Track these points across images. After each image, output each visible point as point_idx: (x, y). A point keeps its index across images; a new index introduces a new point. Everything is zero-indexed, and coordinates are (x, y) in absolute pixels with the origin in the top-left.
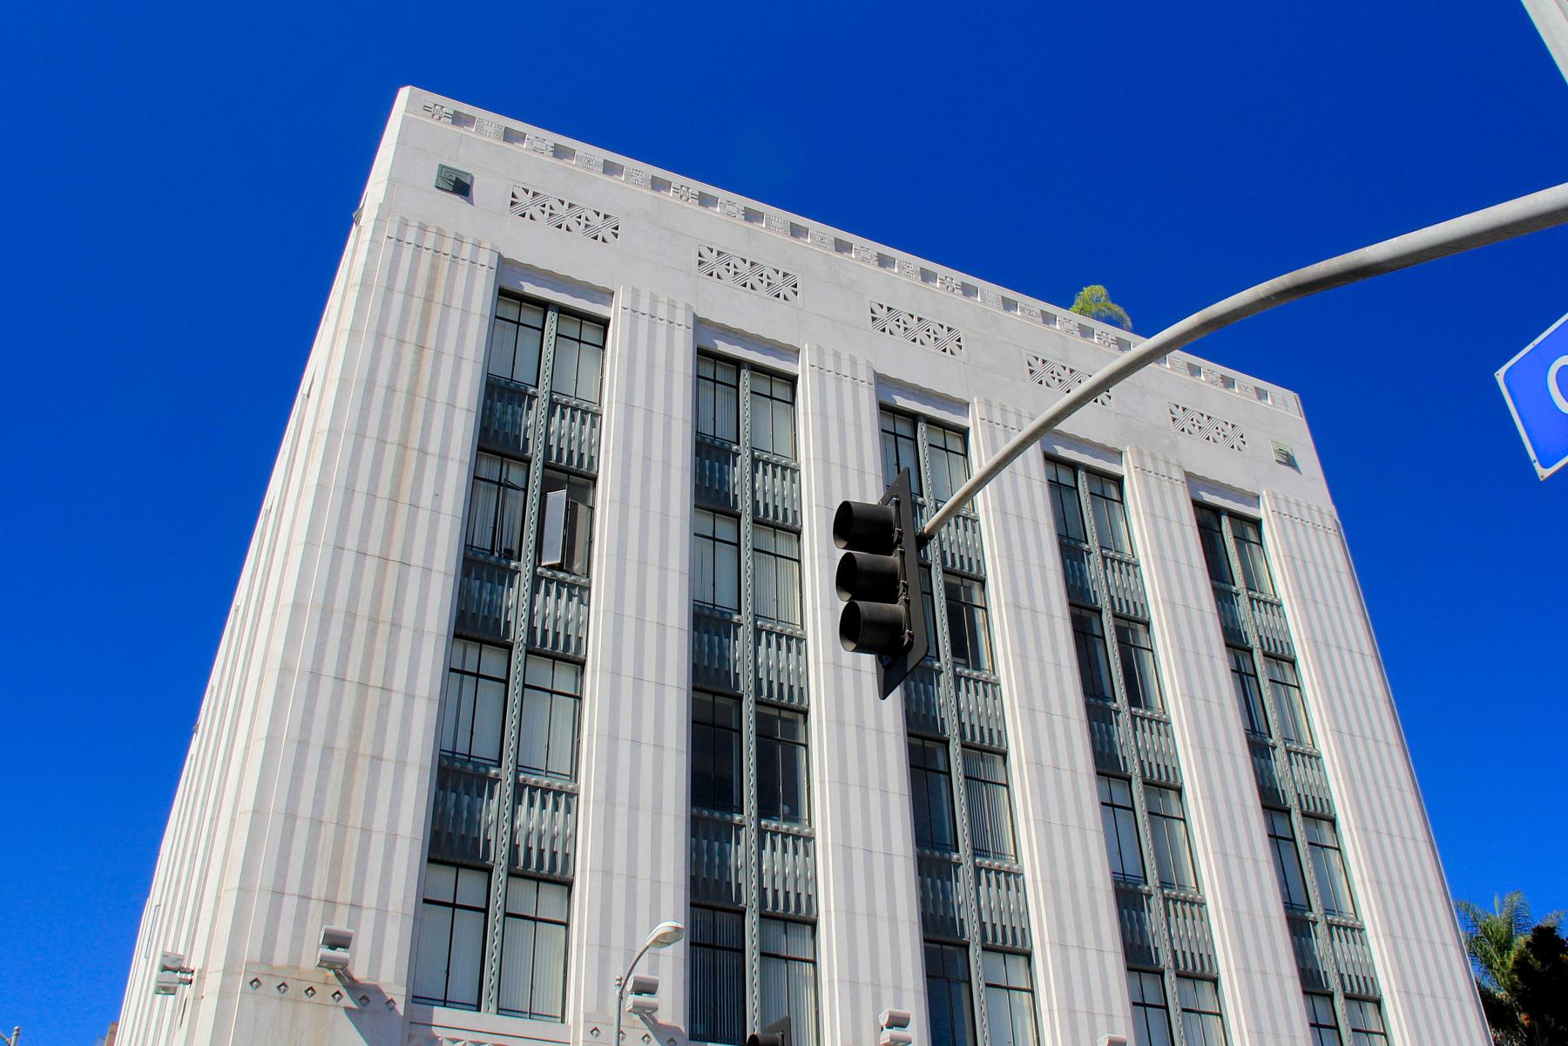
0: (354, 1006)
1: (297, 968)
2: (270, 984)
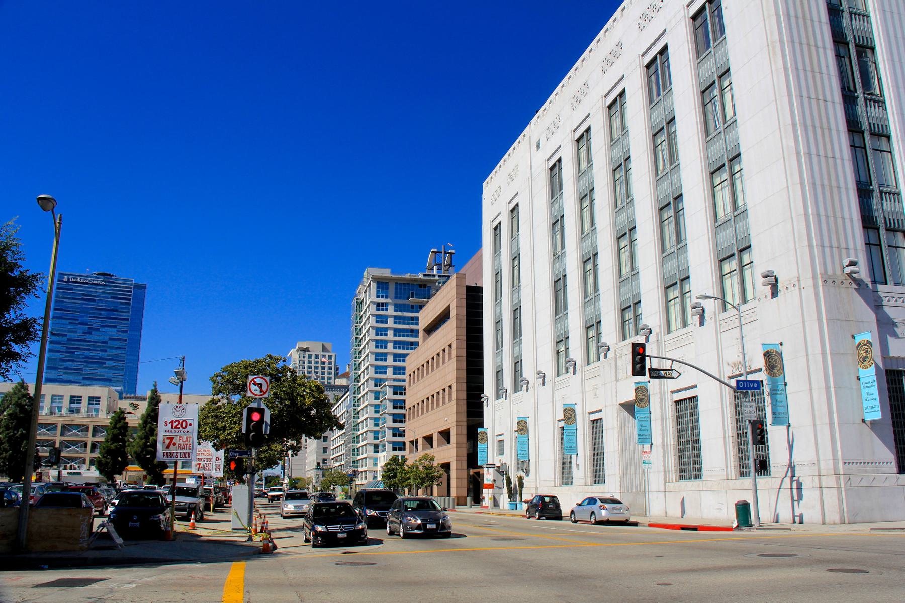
0: (857, 287)
1: (835, 274)
2: (830, 281)
